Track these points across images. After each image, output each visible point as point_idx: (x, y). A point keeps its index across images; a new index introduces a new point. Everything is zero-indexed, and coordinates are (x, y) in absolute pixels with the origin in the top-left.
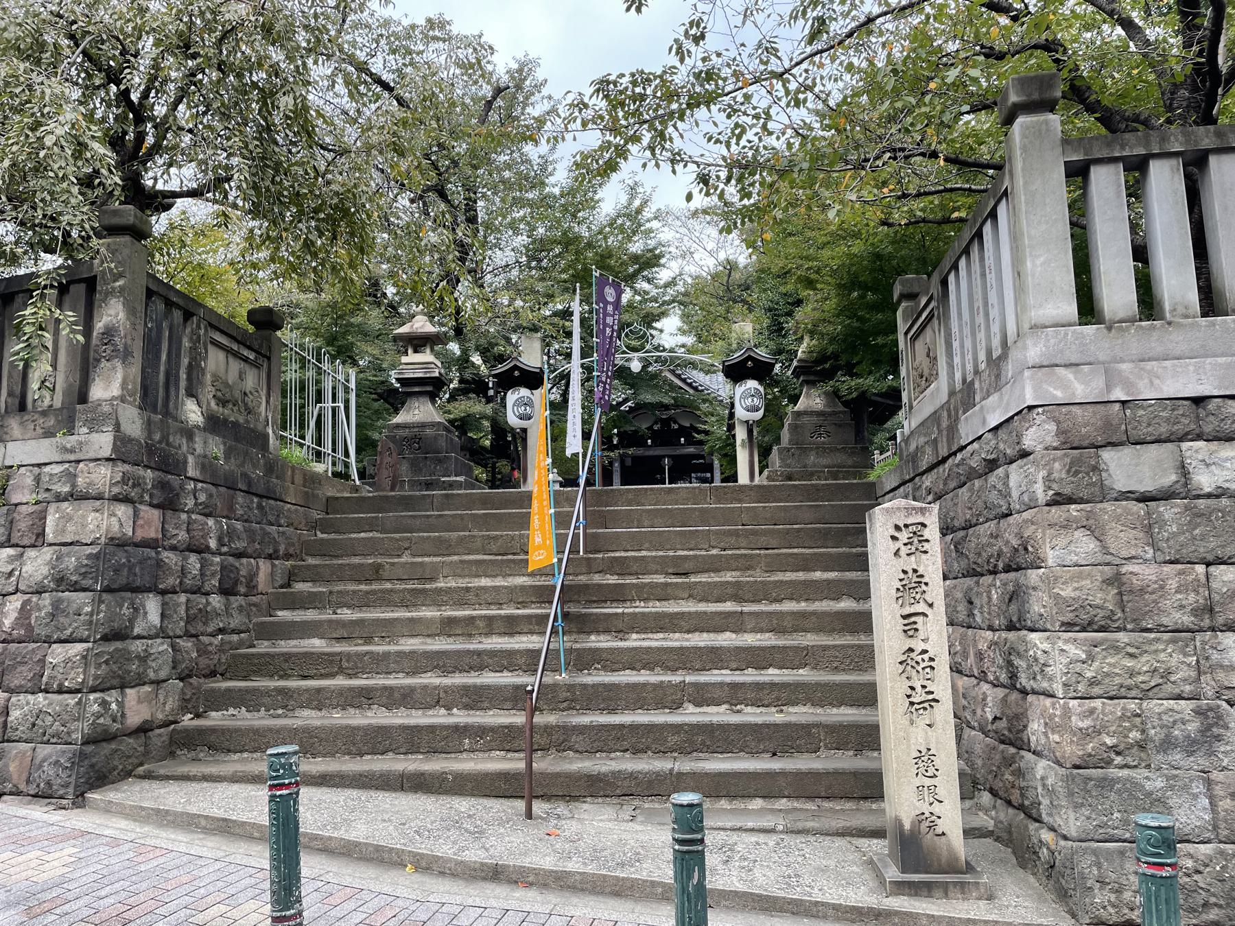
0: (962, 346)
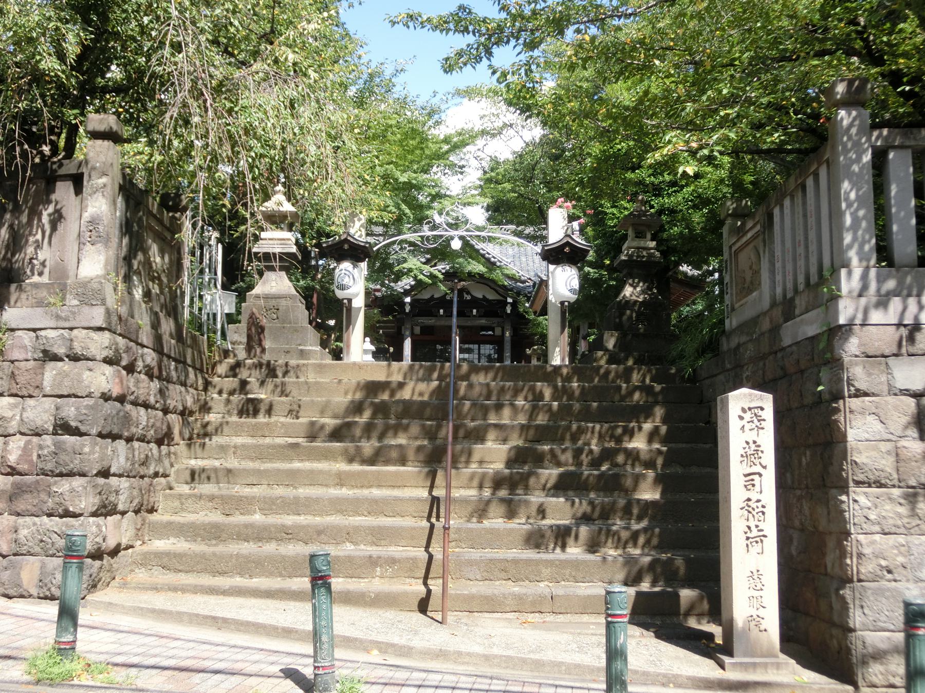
0: (784, 267)
